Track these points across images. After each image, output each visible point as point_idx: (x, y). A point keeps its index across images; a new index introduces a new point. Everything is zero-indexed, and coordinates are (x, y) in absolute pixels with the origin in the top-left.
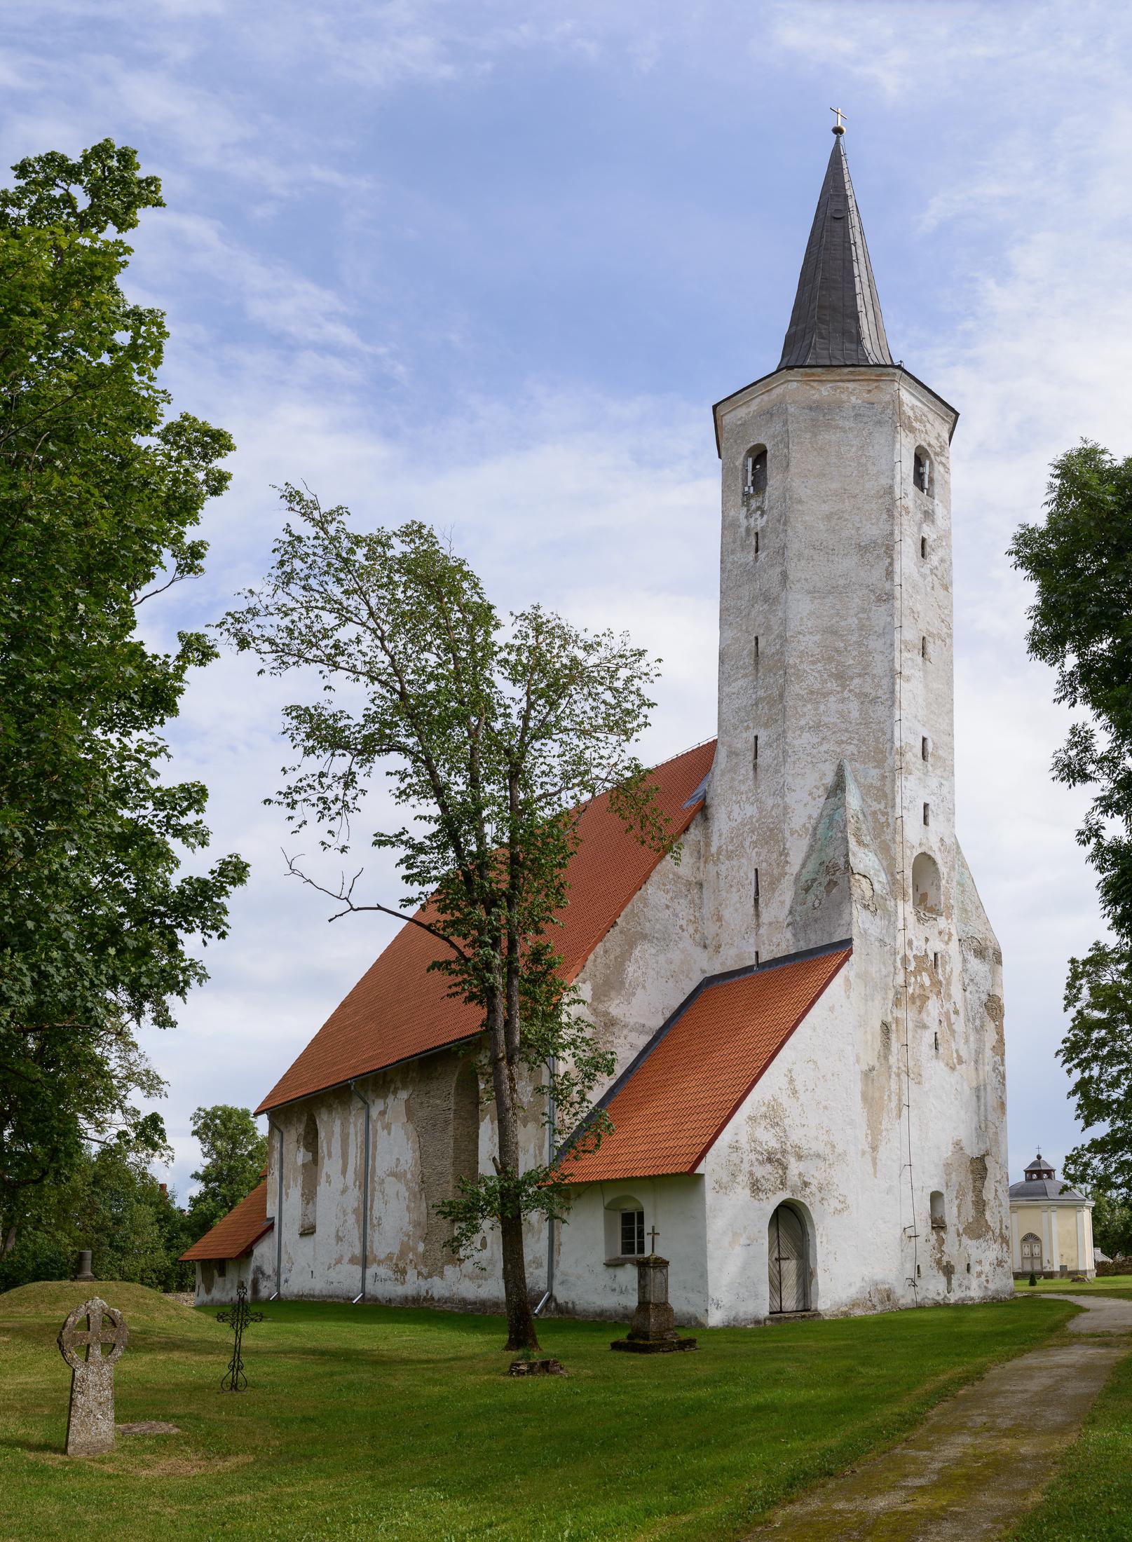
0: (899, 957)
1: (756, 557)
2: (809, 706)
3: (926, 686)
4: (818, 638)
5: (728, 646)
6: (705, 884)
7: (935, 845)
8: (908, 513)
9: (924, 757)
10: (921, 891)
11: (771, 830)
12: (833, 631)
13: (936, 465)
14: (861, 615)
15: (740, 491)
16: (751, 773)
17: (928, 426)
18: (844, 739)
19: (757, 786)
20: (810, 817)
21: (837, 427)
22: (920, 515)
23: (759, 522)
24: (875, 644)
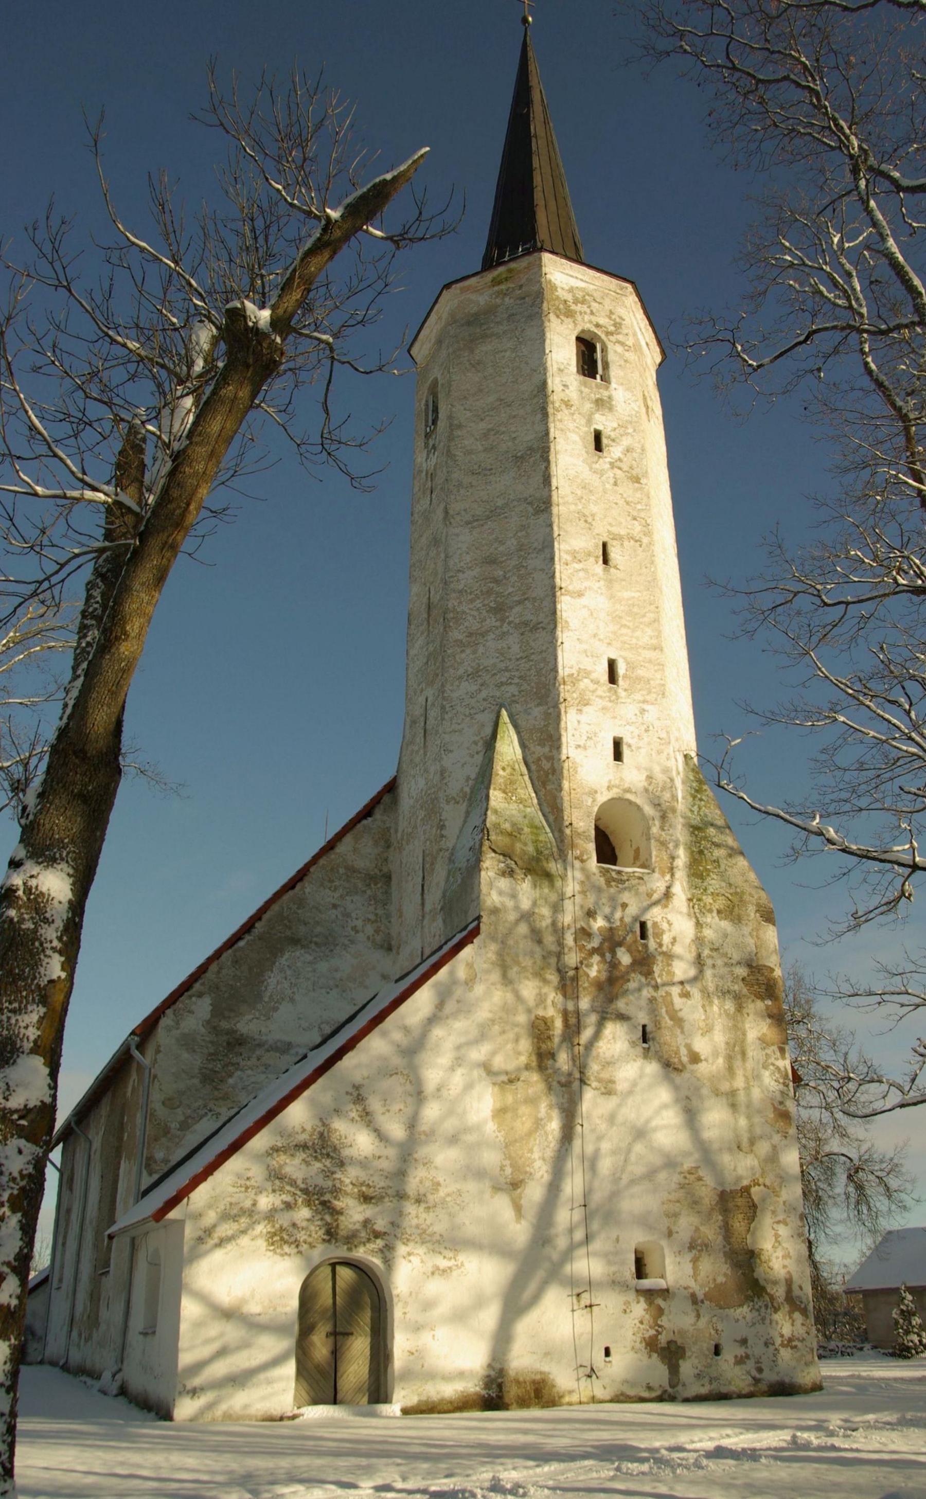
4: (476, 571)
12: (491, 561)
13: (610, 346)
14: (519, 534)
17: (594, 305)
18: (504, 680)
20: (468, 778)
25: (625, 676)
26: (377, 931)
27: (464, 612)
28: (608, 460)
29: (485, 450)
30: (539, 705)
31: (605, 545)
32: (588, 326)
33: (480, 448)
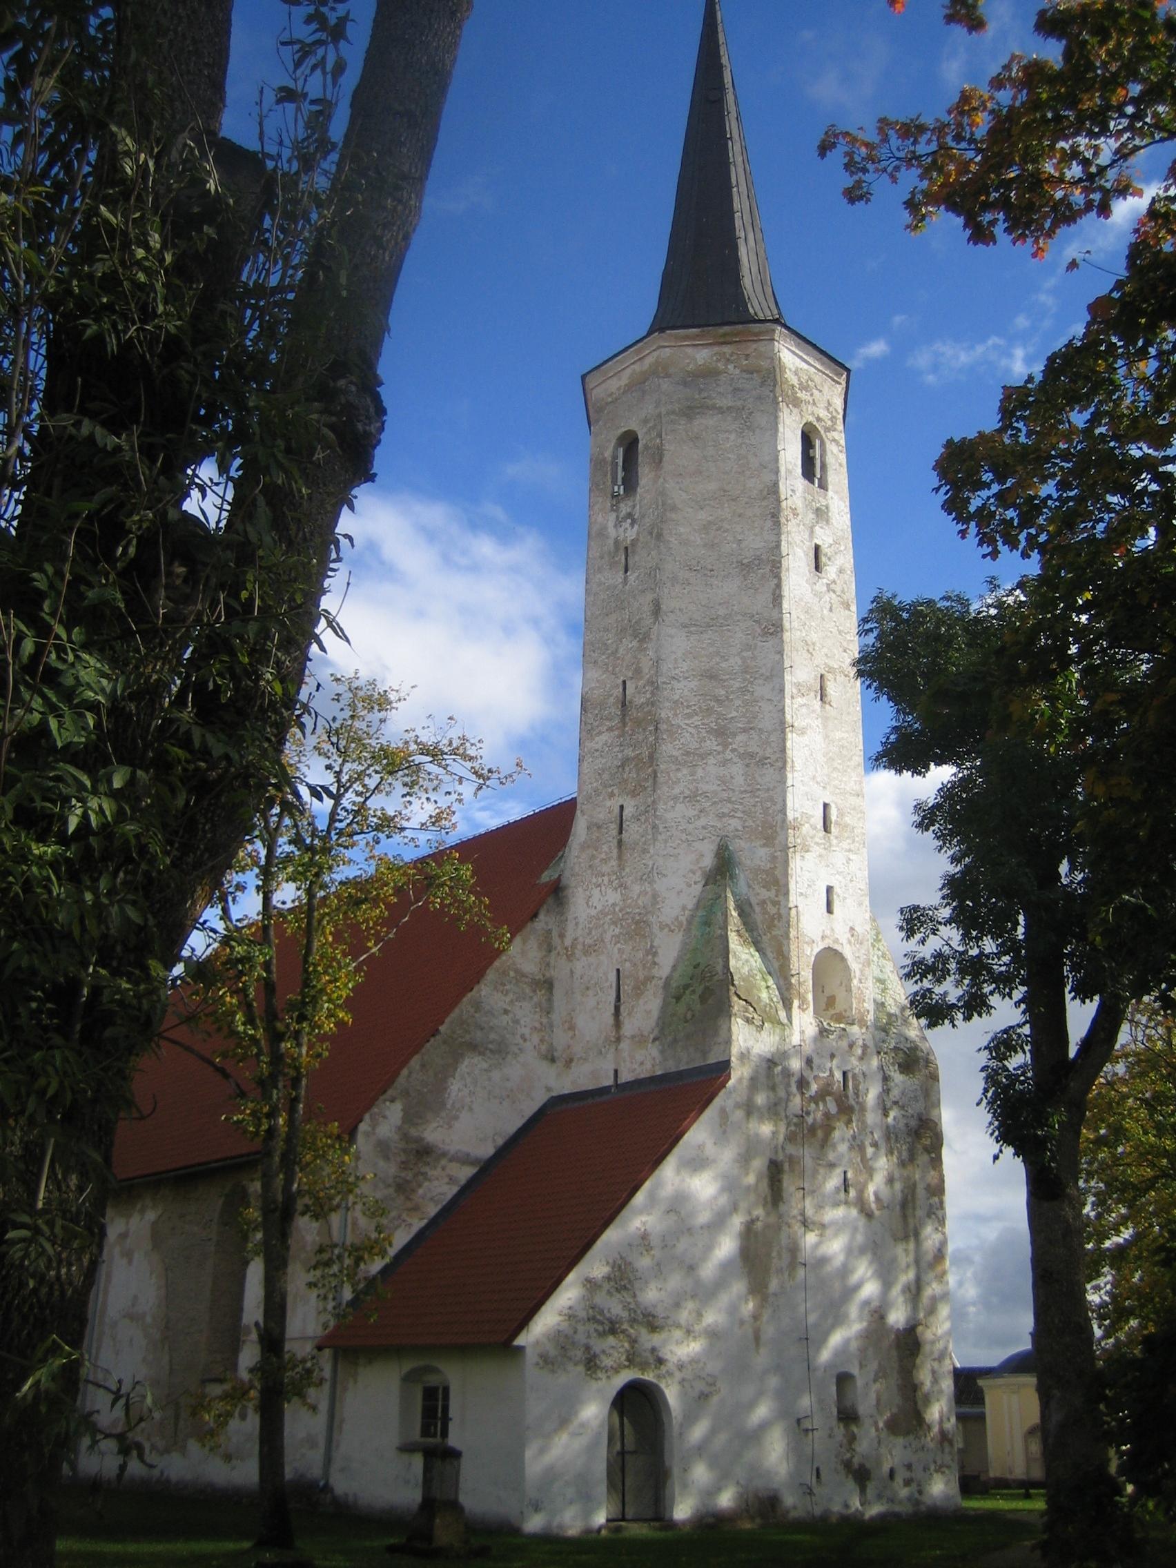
0: (793, 1080)
1: (626, 579)
2: (685, 771)
3: (826, 737)
4: (694, 684)
5: (592, 689)
6: (556, 985)
7: (842, 935)
8: (796, 515)
9: (826, 828)
10: (828, 993)
11: (637, 923)
12: (711, 676)
14: (745, 654)
15: (609, 490)
16: (615, 851)
18: (726, 811)
19: (621, 867)
20: (684, 908)
21: (714, 407)
22: (811, 516)
23: (630, 533)
24: (762, 690)
25: (836, 823)
26: (542, 1041)
27: (679, 726)
28: (825, 581)
29: (705, 545)
30: (764, 845)
31: (822, 676)
32: (811, 419)
33: (699, 541)
